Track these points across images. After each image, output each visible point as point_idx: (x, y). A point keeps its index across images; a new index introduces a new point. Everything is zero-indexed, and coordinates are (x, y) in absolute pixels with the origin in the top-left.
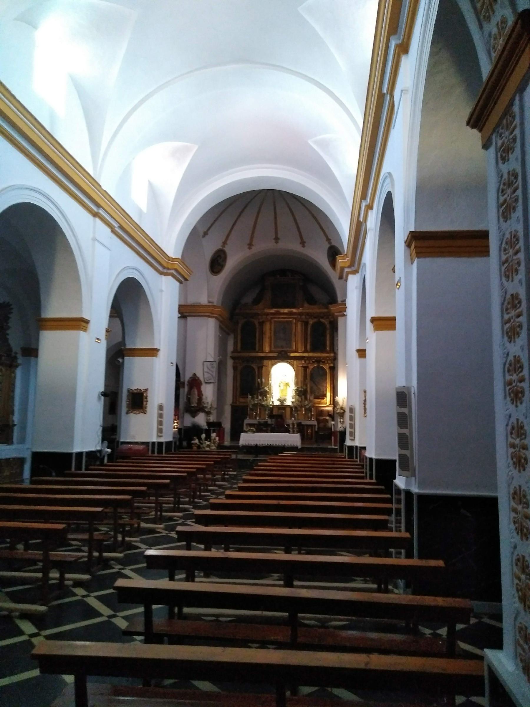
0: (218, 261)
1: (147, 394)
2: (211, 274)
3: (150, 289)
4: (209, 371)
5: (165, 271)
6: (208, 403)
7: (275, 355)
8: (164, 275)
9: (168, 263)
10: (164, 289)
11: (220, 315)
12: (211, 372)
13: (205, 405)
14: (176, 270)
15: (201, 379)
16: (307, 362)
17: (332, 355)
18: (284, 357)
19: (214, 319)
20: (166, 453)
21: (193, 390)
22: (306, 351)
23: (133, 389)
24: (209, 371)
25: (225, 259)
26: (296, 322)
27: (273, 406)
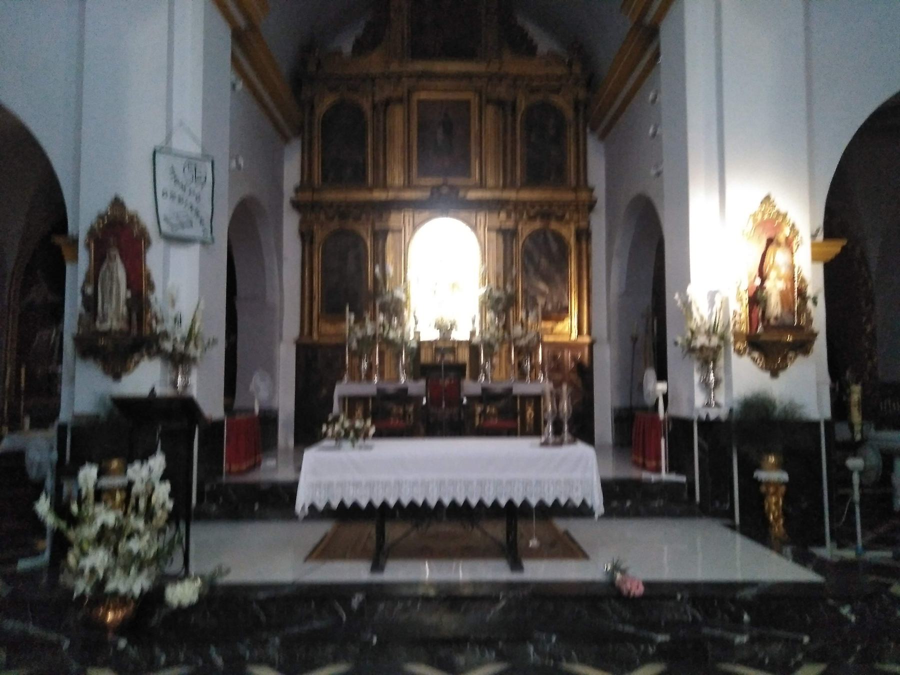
4: (179, 192)
6: (178, 320)
13: (159, 329)
15: (147, 220)
24: (179, 192)
27: (420, 344)
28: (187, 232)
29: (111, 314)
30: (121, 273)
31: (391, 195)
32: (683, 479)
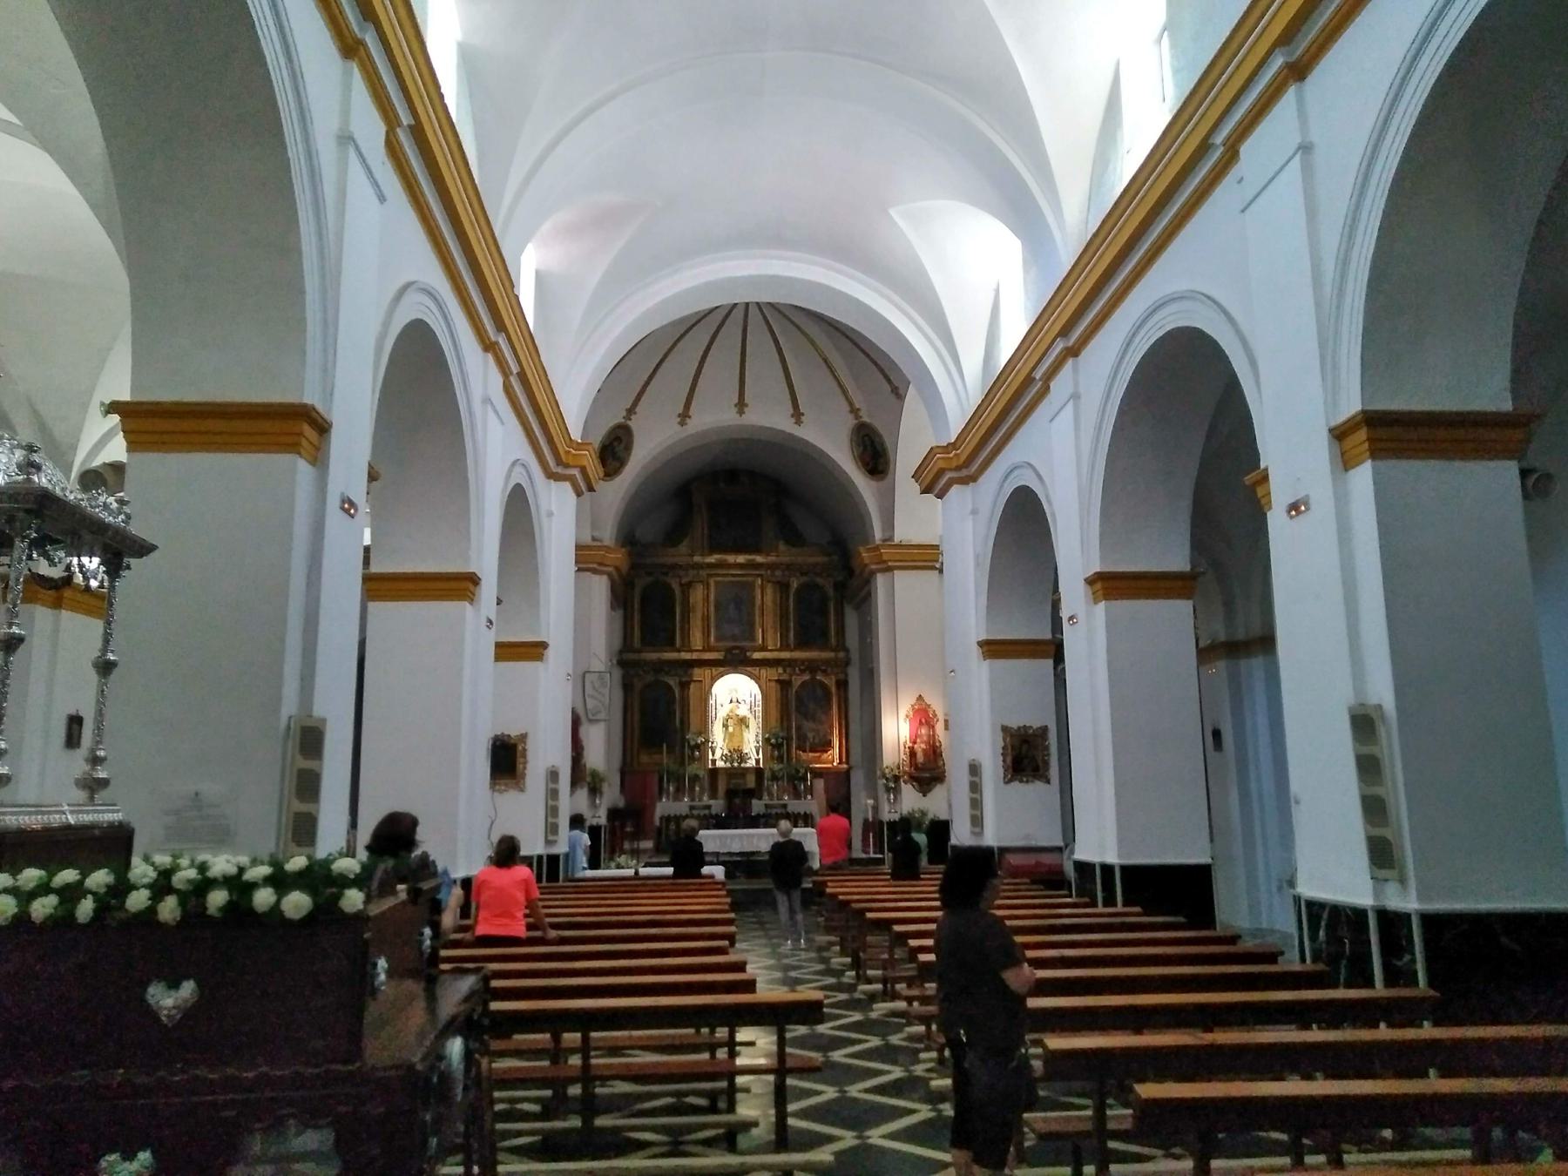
3: (1053, 515)
8: (555, 480)
10: (554, 508)
14: (583, 470)
16: (788, 670)
17: (841, 655)
18: (737, 661)
22: (785, 646)
25: (628, 448)
26: (762, 583)
28: (598, 717)
31: (695, 656)
32: (881, 856)
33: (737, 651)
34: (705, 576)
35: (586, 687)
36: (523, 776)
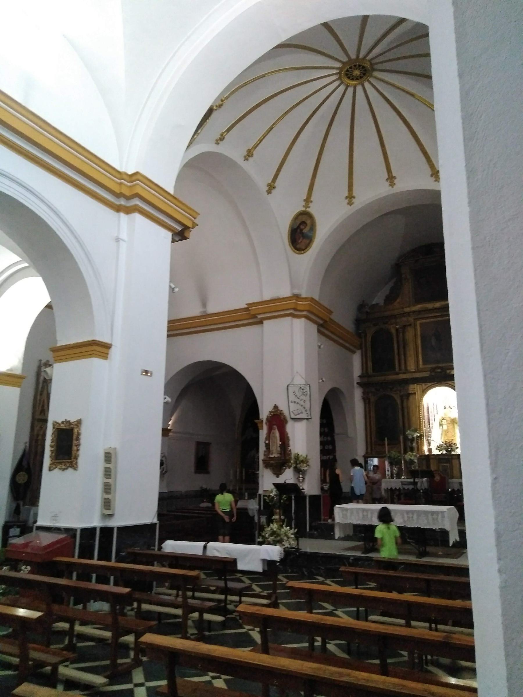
0: (301, 230)
1: (80, 429)
2: (294, 251)
4: (297, 400)
5: (122, 202)
7: (426, 374)
9: (121, 184)
11: (308, 311)
12: (302, 403)
15: (286, 412)
19: (303, 320)
20: (79, 557)
21: (273, 431)
23: (60, 422)
24: (297, 400)
29: (274, 451)
30: (277, 434)
33: (439, 370)
34: (413, 321)
35: (290, 396)
36: (76, 458)
